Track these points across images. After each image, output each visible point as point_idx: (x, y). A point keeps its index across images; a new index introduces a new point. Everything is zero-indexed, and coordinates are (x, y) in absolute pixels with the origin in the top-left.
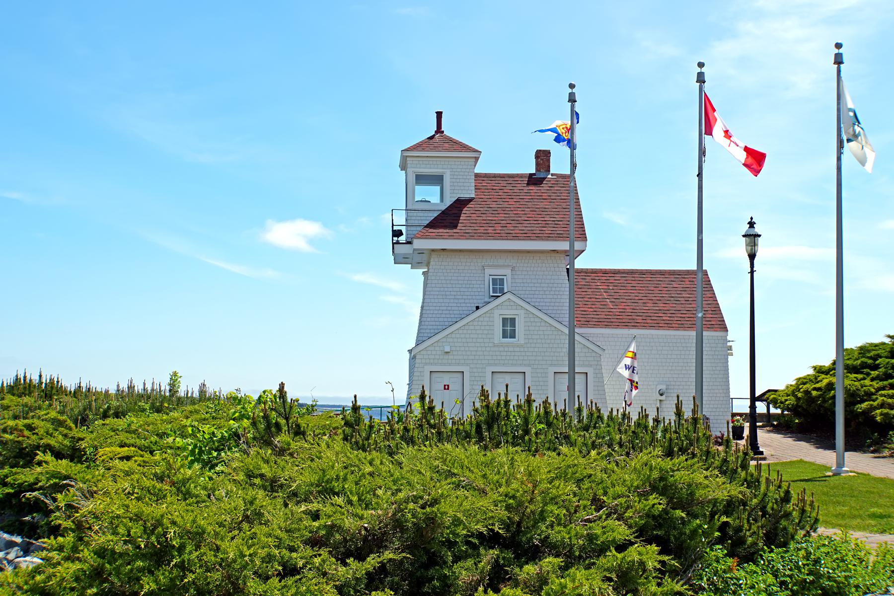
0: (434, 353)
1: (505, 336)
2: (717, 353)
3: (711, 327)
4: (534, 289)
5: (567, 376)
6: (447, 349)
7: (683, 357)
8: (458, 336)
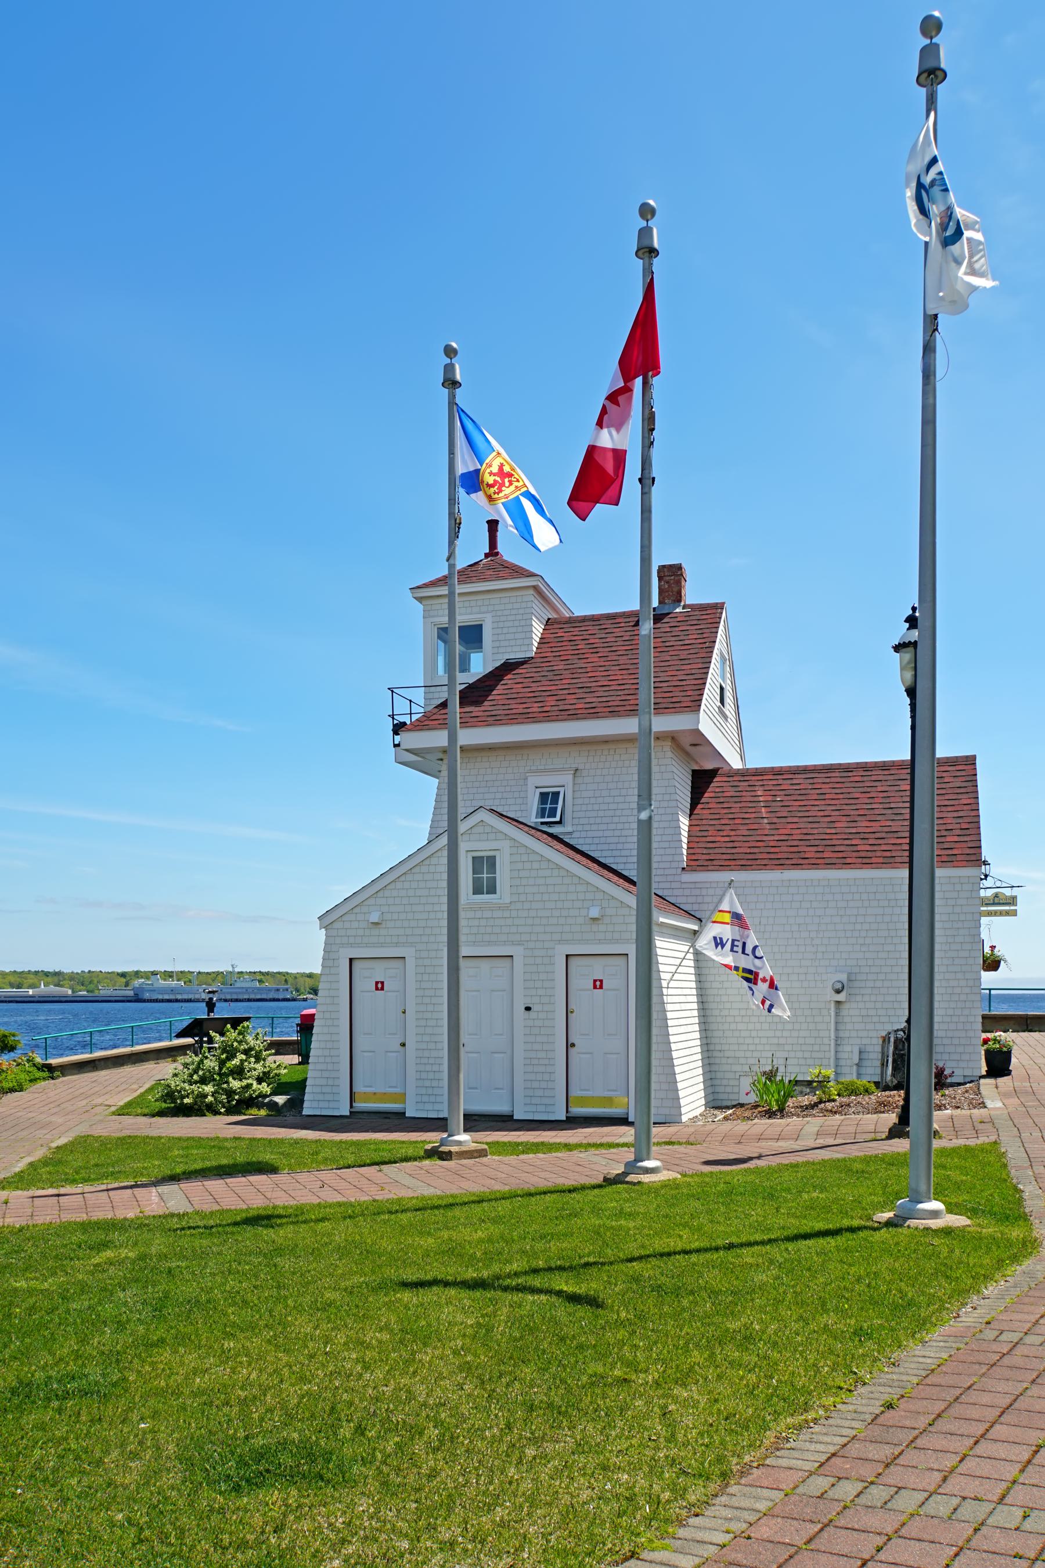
0: (355, 925)
1: (477, 890)
2: (957, 910)
3: (950, 860)
4: (612, 806)
6: (375, 917)
7: (887, 919)
8: (395, 893)
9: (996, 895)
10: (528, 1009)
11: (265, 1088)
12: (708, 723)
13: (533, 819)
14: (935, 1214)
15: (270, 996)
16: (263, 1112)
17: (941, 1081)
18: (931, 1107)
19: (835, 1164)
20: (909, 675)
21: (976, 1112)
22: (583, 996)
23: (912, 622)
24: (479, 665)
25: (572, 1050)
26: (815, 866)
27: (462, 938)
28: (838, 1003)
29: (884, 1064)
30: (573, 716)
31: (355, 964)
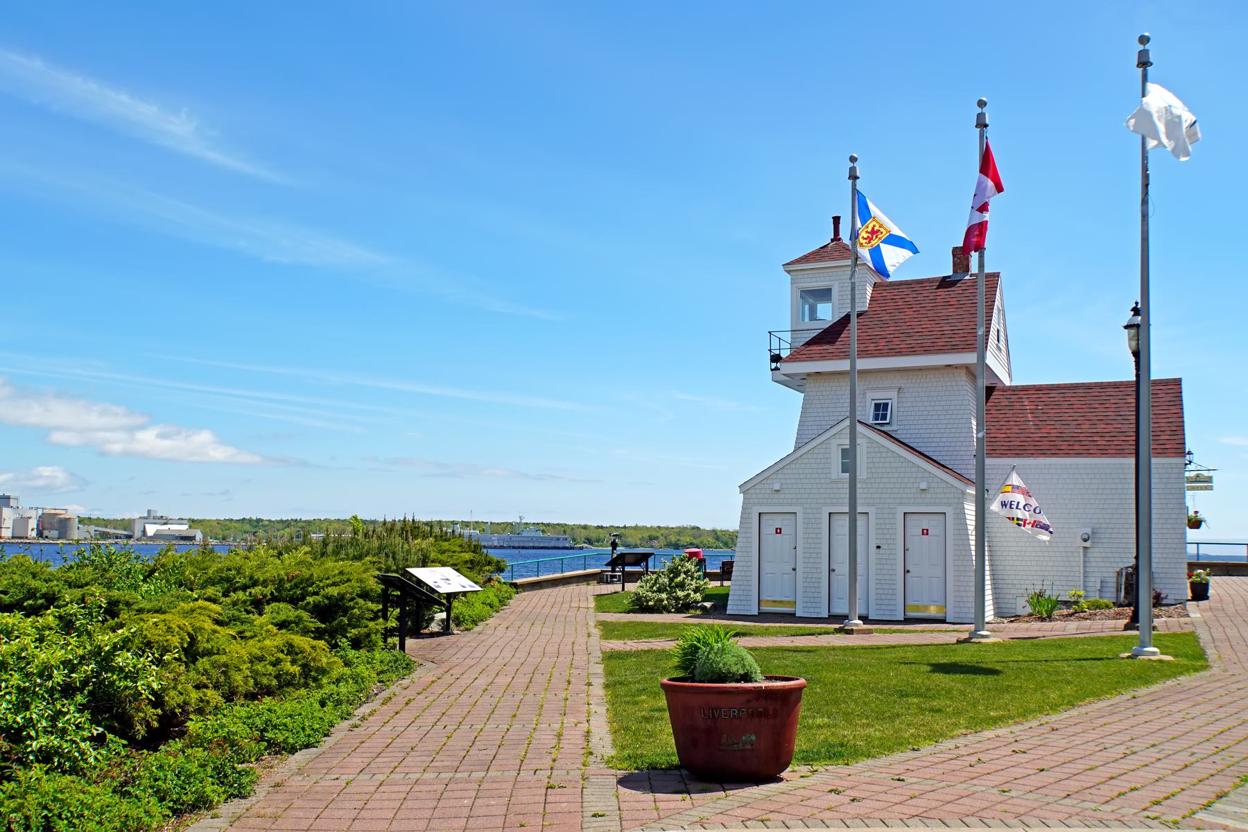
3: (1162, 452)
5: (847, 518)
6: (777, 487)
9: (1198, 476)
10: (878, 547)
11: (698, 596)
12: (993, 360)
13: (871, 421)
14: (1154, 653)
15: (552, 544)
16: (699, 612)
17: (1158, 601)
18: (1152, 617)
19: (1091, 639)
20: (1134, 343)
21: (1182, 620)
22: (916, 540)
23: (1136, 311)
24: (827, 314)
25: (908, 575)
26: (1068, 455)
27: (859, 501)
28: (1085, 548)
29: (1118, 590)
30: (899, 353)
31: (764, 518)
